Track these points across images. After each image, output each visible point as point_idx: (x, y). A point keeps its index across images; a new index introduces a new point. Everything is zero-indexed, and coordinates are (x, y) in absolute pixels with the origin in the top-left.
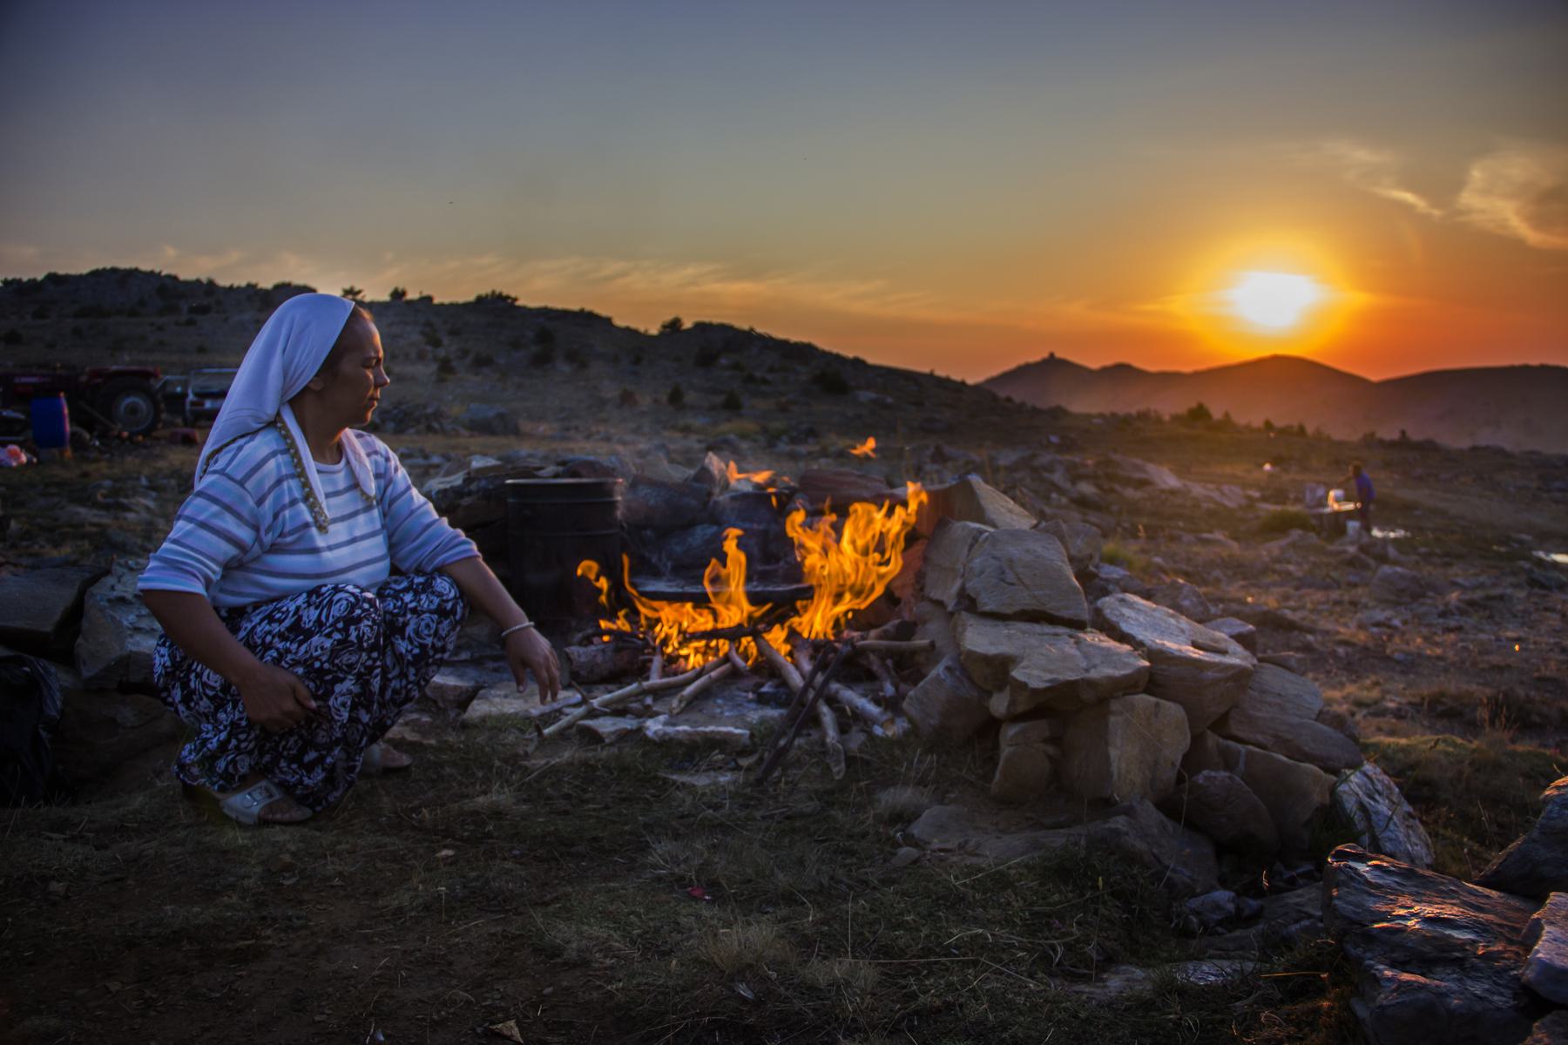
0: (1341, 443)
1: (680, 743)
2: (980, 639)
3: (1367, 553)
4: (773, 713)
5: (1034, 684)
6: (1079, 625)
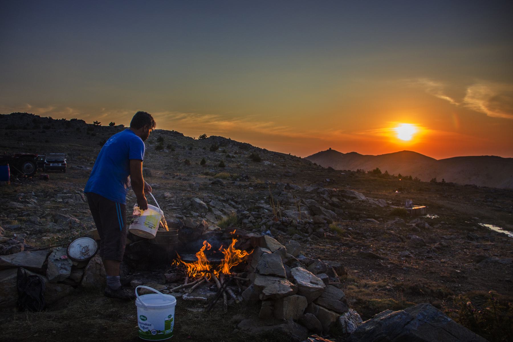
0: (422, 183)
1: (191, 301)
2: (258, 281)
3: (418, 227)
4: (213, 293)
5: (267, 294)
6: (283, 277)
